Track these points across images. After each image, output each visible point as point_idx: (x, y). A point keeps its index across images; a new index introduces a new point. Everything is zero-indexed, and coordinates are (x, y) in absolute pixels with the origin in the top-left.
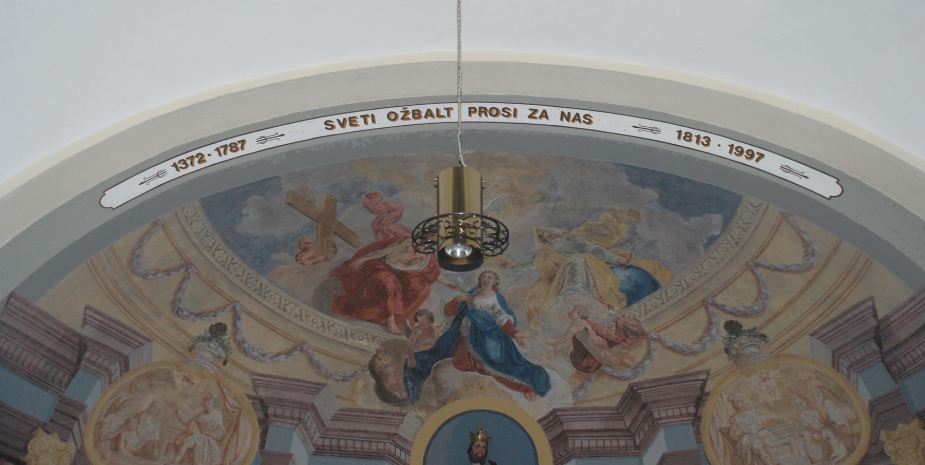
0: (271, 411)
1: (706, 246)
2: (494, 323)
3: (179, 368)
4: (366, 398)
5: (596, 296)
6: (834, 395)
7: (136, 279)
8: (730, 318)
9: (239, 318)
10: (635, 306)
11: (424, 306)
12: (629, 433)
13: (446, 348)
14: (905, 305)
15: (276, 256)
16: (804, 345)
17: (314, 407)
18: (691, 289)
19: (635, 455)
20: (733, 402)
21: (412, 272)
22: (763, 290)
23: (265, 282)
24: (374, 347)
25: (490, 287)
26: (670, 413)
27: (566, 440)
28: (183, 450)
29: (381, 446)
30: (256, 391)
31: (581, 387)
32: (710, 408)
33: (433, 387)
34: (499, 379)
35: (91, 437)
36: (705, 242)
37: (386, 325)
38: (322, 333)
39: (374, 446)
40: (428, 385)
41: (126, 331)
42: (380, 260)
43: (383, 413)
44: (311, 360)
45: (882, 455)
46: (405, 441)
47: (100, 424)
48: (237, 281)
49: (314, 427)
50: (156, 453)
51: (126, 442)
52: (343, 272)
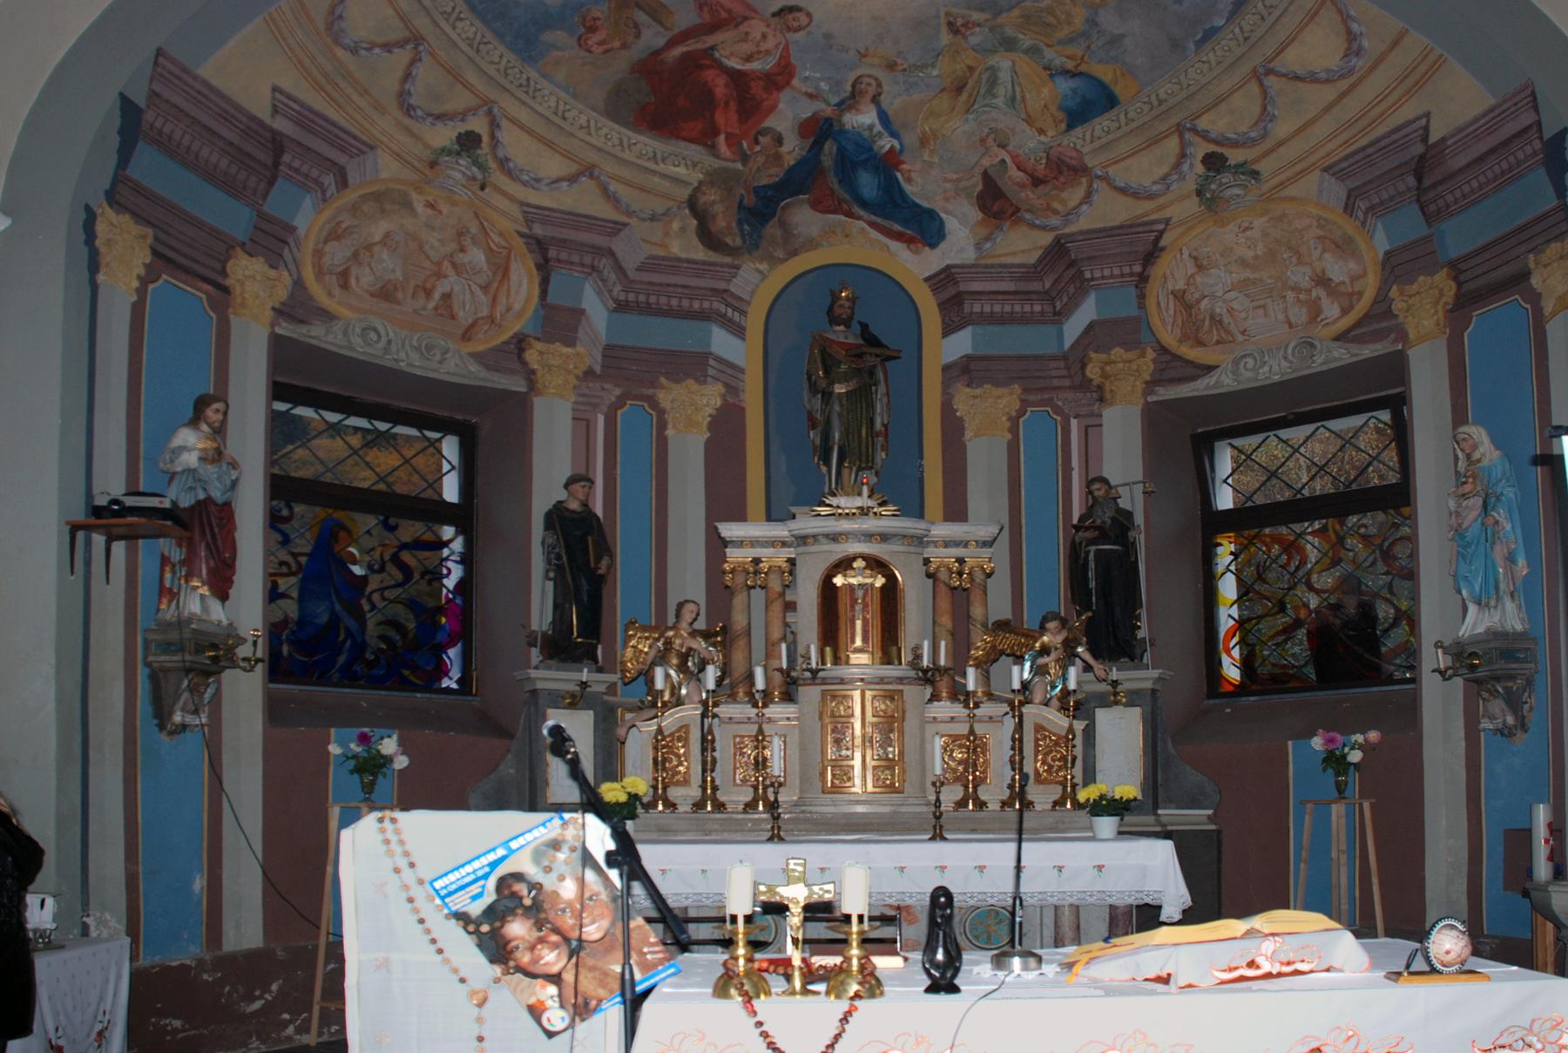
0: (552, 253)
1: (1199, 44)
2: (871, 149)
3: (420, 191)
4: (684, 245)
5: (1023, 115)
6: (1338, 247)
7: (340, 53)
8: (1212, 148)
9: (498, 126)
10: (1078, 131)
11: (770, 122)
12: (1048, 296)
13: (800, 181)
14: (1476, 120)
15: (548, 37)
16: (1310, 184)
17: (611, 253)
18: (1163, 108)
19: (1053, 322)
20: (1195, 259)
21: (753, 72)
22: (1269, 108)
23: (534, 74)
24: (695, 177)
25: (868, 97)
26: (1107, 272)
27: (961, 304)
28: (437, 295)
29: (706, 305)
30: (530, 228)
31: (987, 239)
32: (1162, 266)
33: (779, 233)
34: (872, 225)
35: (310, 268)
36: (1199, 36)
37: (712, 148)
38: (620, 154)
39: (696, 305)
40: (772, 230)
41: (336, 131)
42: (705, 51)
43: (705, 263)
44: (605, 190)
45: (1389, 314)
46: (742, 299)
47: (319, 254)
48: (491, 70)
49: (613, 277)
50: (400, 295)
51: (357, 279)
52: (648, 68)
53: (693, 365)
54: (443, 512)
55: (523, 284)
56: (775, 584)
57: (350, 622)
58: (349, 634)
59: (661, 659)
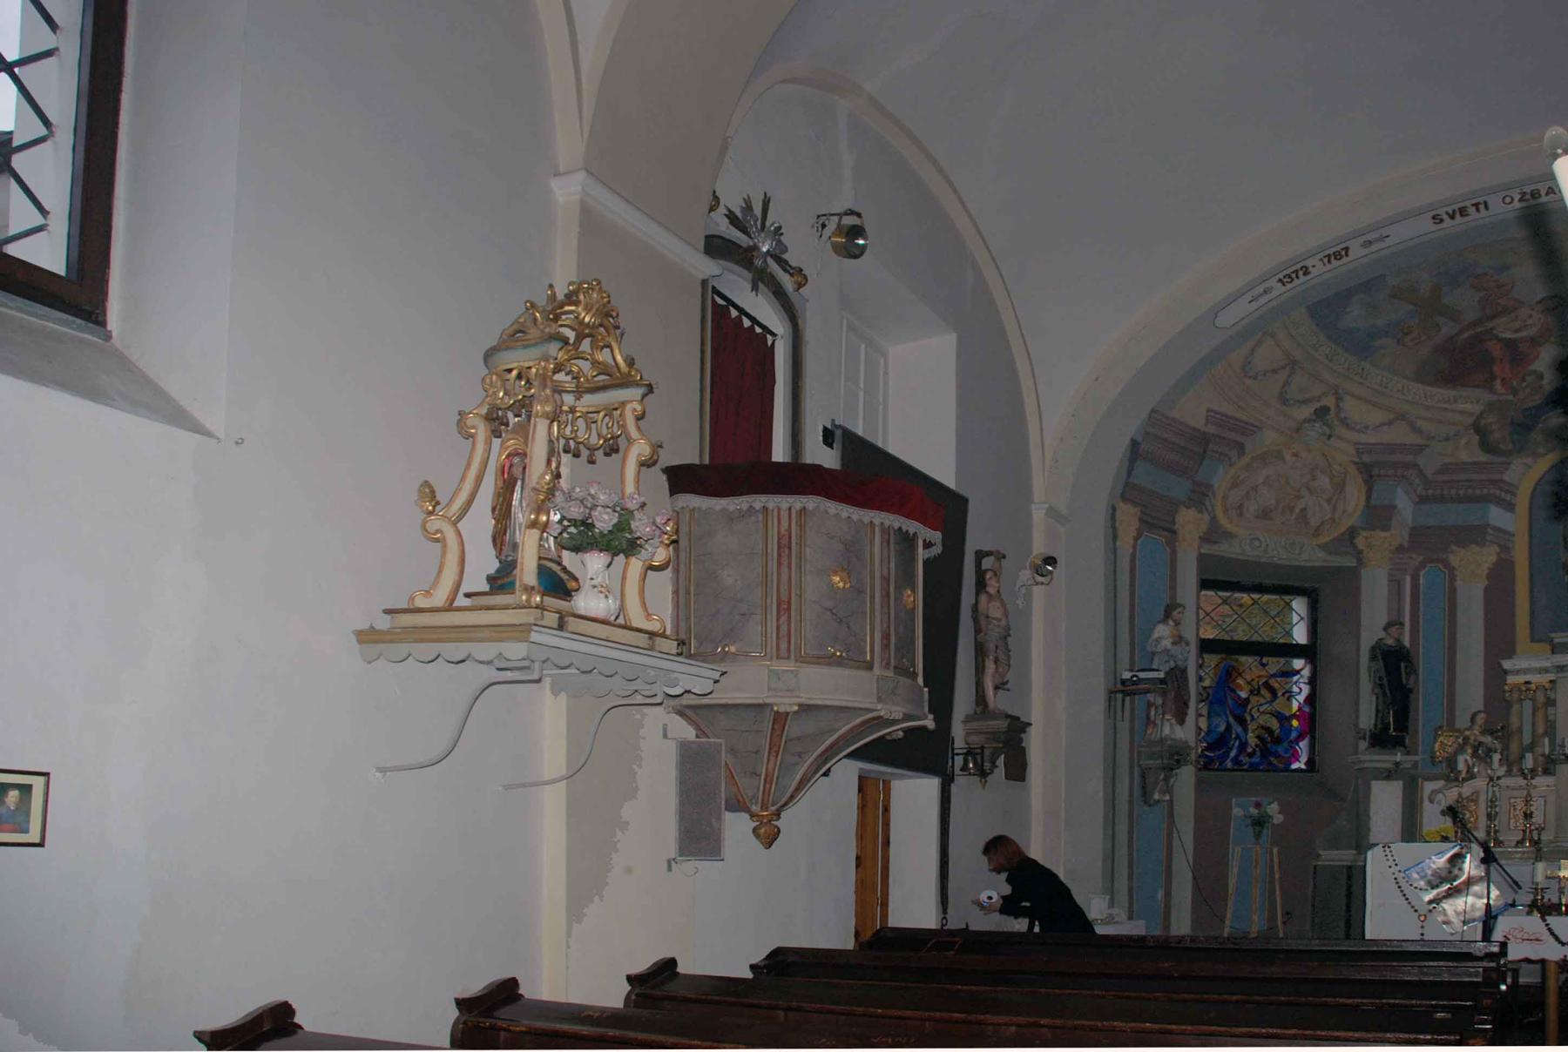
0: (1375, 471)
4: (1468, 452)
7: (1248, 381)
11: (1532, 367)
17: (1416, 465)
24: (1478, 409)
37: (1491, 390)
47: (1225, 498)
53: (1473, 534)
54: (1294, 650)
55: (1354, 496)
56: (1541, 698)
57: (1238, 729)
58: (1238, 737)
59: (1461, 749)
